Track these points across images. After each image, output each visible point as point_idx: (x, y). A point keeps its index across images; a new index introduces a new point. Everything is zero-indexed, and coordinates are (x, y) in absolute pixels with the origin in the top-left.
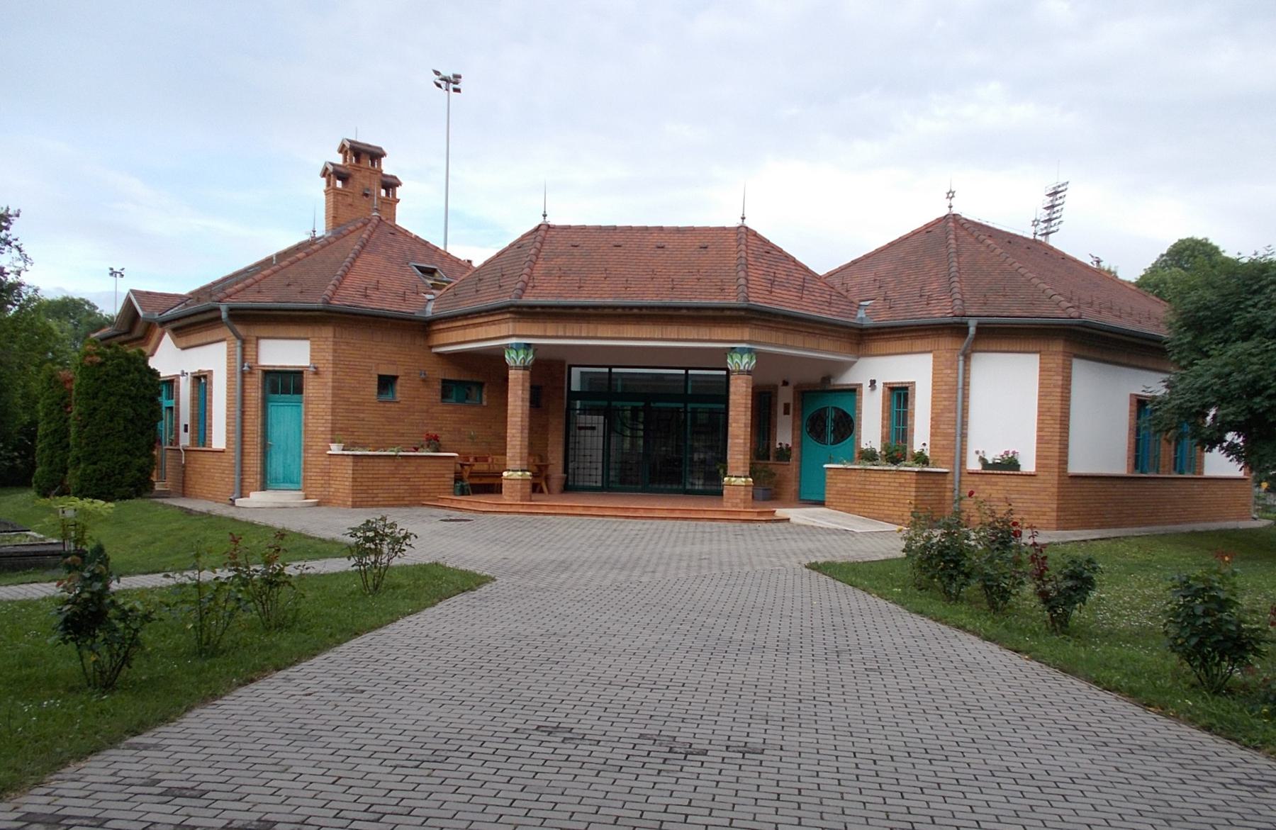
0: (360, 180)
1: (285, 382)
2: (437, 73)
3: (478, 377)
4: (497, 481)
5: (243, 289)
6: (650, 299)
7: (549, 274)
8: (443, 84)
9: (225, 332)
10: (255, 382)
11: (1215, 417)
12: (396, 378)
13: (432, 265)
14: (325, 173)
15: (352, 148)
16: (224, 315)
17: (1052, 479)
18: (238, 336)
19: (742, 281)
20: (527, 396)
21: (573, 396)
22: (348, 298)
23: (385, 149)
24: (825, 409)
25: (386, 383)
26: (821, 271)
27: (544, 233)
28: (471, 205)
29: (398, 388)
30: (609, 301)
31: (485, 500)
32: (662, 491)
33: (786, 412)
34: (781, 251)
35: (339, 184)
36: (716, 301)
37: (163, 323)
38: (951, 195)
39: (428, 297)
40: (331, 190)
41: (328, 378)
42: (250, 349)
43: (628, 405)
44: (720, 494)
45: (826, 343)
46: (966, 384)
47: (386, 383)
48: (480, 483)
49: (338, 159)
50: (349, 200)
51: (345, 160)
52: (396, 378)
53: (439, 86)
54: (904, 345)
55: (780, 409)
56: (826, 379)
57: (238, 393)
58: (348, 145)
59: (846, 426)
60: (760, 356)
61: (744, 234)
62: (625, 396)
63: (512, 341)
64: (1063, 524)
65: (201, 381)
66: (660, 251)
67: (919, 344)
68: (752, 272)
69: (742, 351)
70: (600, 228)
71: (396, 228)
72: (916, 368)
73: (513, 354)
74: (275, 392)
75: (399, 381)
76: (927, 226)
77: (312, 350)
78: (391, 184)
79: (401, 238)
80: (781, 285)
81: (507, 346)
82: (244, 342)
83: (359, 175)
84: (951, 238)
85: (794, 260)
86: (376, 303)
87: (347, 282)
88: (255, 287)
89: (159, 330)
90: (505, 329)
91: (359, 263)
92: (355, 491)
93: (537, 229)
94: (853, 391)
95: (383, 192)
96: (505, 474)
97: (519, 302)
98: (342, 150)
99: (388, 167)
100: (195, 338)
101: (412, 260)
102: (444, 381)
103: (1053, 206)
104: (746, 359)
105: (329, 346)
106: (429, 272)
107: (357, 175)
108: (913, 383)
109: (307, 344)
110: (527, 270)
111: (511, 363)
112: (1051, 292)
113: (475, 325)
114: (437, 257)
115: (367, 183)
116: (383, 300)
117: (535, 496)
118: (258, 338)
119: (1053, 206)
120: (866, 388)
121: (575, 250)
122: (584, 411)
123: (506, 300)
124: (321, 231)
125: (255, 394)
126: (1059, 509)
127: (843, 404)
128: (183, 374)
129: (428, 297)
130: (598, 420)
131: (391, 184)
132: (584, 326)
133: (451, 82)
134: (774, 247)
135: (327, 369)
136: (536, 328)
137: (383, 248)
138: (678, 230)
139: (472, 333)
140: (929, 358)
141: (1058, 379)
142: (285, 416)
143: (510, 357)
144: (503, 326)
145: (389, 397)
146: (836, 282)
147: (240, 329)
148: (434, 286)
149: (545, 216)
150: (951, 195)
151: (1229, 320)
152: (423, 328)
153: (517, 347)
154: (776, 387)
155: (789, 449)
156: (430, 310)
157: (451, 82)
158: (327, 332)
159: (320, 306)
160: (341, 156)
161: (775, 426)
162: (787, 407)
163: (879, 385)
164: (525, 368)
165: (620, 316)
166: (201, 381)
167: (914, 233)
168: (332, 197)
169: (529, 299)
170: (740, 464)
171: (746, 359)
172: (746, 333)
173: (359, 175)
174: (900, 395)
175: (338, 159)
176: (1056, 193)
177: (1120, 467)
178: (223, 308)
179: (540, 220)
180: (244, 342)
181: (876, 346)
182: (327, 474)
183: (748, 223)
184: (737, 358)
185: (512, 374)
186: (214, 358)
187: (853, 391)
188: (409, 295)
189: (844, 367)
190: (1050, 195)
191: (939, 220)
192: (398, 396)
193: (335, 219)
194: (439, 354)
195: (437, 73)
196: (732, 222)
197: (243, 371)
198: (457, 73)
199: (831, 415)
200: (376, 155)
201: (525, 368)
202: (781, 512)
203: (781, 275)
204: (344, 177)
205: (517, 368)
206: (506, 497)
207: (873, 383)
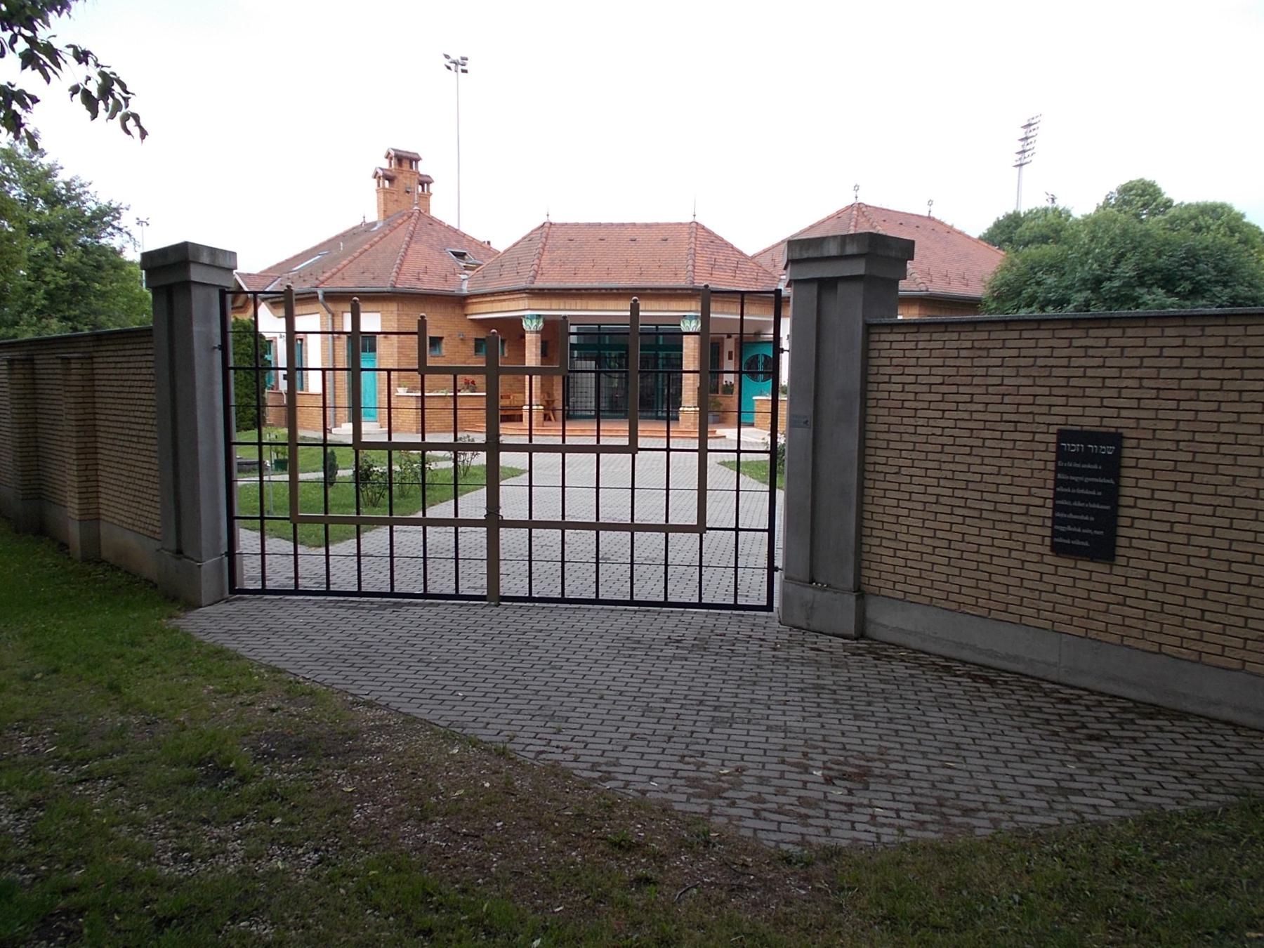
0: (403, 181)
2: (447, 57)
4: (518, 413)
5: (331, 277)
6: (623, 284)
7: (552, 264)
8: (452, 66)
12: (441, 338)
13: (464, 252)
15: (396, 156)
16: (320, 297)
18: (329, 312)
19: (690, 268)
24: (757, 357)
26: (750, 253)
27: (547, 229)
28: (492, 205)
30: (596, 285)
33: (730, 358)
34: (722, 240)
36: (671, 284)
38: (856, 188)
39: (463, 277)
42: (337, 320)
43: (614, 354)
49: (385, 164)
50: (395, 197)
52: (441, 338)
53: (449, 68)
55: (726, 356)
61: (696, 228)
62: (611, 347)
66: (633, 244)
69: (691, 318)
70: (589, 224)
71: (431, 218)
73: (529, 322)
76: (839, 213)
77: (383, 320)
78: (425, 182)
79: (437, 227)
80: (720, 267)
82: (333, 315)
83: (401, 172)
85: (732, 247)
86: (427, 285)
87: (404, 268)
88: (339, 274)
91: (410, 252)
97: (533, 286)
98: (388, 156)
99: (423, 168)
101: (448, 246)
102: (476, 340)
103: (1027, 138)
106: (460, 256)
107: (400, 177)
109: (379, 315)
110: (537, 261)
113: (500, 301)
114: (465, 243)
115: (408, 182)
116: (431, 281)
117: (546, 423)
119: (1027, 138)
121: (571, 244)
122: (579, 358)
123: (523, 284)
124: (373, 215)
129: (463, 277)
130: (591, 365)
131: (425, 182)
133: (459, 65)
134: (717, 237)
136: (544, 304)
137: (425, 238)
138: (647, 226)
139: (497, 306)
143: (526, 325)
145: (437, 353)
146: (761, 260)
147: (330, 305)
148: (466, 268)
150: (856, 188)
151: (1020, 293)
152: (460, 301)
153: (531, 317)
155: (732, 385)
156: (465, 288)
157: (459, 65)
158: (393, 307)
159: (390, 289)
160: (387, 161)
162: (730, 353)
164: (537, 332)
165: (604, 294)
167: (829, 218)
168: (382, 196)
169: (539, 284)
170: (691, 398)
175: (385, 164)
176: (1030, 125)
178: (320, 292)
179: (545, 219)
183: (698, 220)
184: (687, 323)
188: (450, 277)
190: (1025, 127)
191: (848, 208)
192: (444, 352)
193: (385, 213)
195: (447, 57)
198: (464, 55)
199: (761, 359)
200: (413, 159)
201: (537, 332)
203: (721, 259)
204: (391, 179)
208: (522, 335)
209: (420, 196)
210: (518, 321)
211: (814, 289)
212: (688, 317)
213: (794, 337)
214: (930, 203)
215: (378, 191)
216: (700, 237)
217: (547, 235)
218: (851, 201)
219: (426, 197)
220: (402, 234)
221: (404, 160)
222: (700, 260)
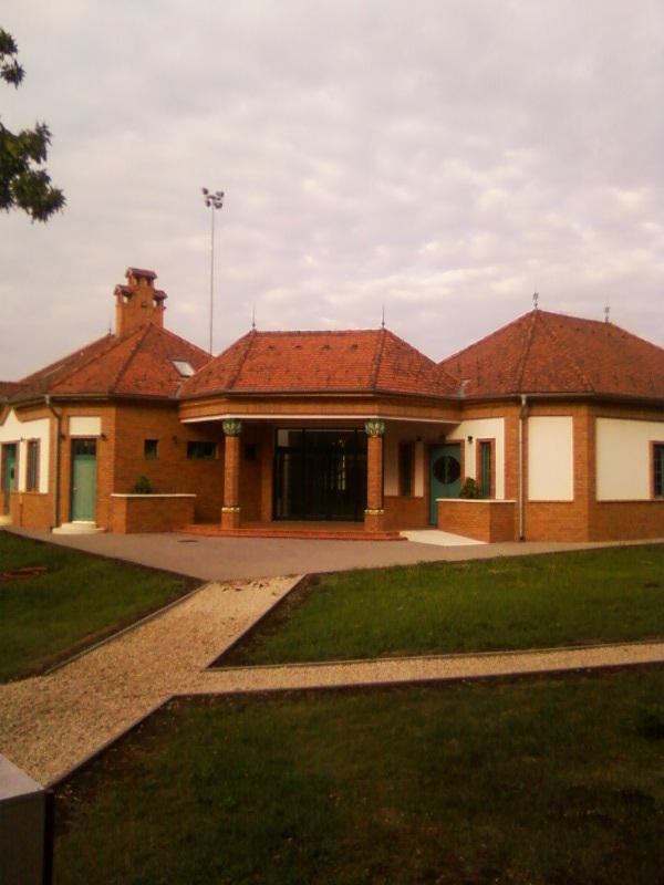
0: (140, 297)
1: (84, 447)
3: (207, 440)
9: (47, 412)
10: (66, 445)
11: (347, 462)
14: (116, 293)
16: (48, 402)
17: (583, 508)
18: (56, 415)
19: (373, 372)
20: (237, 454)
21: (281, 450)
22: (129, 387)
23: (157, 272)
25: (150, 445)
27: (253, 339)
29: (158, 449)
31: (210, 529)
32: (342, 520)
35: (125, 299)
37: (11, 404)
40: (120, 304)
41: (112, 443)
44: (362, 520)
45: (436, 412)
46: (525, 439)
47: (150, 445)
48: (206, 515)
49: (125, 282)
51: (130, 282)
54: (487, 411)
56: (443, 437)
57: (55, 479)
58: (131, 272)
59: (456, 468)
60: (387, 423)
61: (384, 335)
63: (226, 415)
64: (592, 538)
65: (33, 445)
67: (496, 411)
68: (383, 364)
72: (491, 428)
73: (228, 426)
74: (79, 453)
75: (158, 444)
78: (160, 297)
81: (224, 420)
83: (140, 291)
84: (538, 327)
89: (6, 409)
90: (222, 408)
92: (128, 522)
93: (248, 336)
94: (459, 445)
95: (155, 303)
96: (224, 509)
99: (158, 285)
100: (30, 415)
104: (377, 426)
105: (112, 420)
108: (494, 439)
111: (227, 432)
112: (579, 372)
116: (147, 388)
118: (69, 417)
120: (467, 442)
125: (66, 455)
126: (590, 527)
127: (451, 453)
128: (22, 440)
131: (160, 297)
132: (272, 406)
135: (111, 436)
140: (502, 420)
141: (585, 434)
142: (84, 468)
144: (223, 406)
147: (58, 410)
149: (254, 325)
153: (230, 421)
154: (463, 441)
157: (215, 201)
161: (414, 470)
163: (474, 440)
166: (33, 445)
169: (237, 389)
171: (377, 426)
172: (376, 408)
173: (140, 291)
174: (486, 447)
175: (125, 282)
177: (569, 495)
178: (47, 397)
179: (251, 328)
180: (60, 418)
181: (471, 413)
182: (110, 510)
184: (371, 425)
185: (228, 439)
186: (40, 429)
187: (459, 445)
189: (453, 427)
192: (158, 453)
193: (123, 321)
194: (186, 424)
196: (377, 327)
197: (61, 436)
198: (220, 190)
200: (149, 277)
201: (236, 435)
202: (403, 534)
205: (230, 436)
206: (226, 526)
207: (470, 438)
208: (222, 436)
209: (155, 310)
210: (219, 424)
211: (527, 536)
212: (371, 417)
213: (434, 571)
214: (607, 310)
215: (117, 306)
216: (388, 346)
217: (253, 342)
218: (531, 309)
219: (160, 309)
220: (130, 345)
221: (142, 278)
222: (385, 366)
